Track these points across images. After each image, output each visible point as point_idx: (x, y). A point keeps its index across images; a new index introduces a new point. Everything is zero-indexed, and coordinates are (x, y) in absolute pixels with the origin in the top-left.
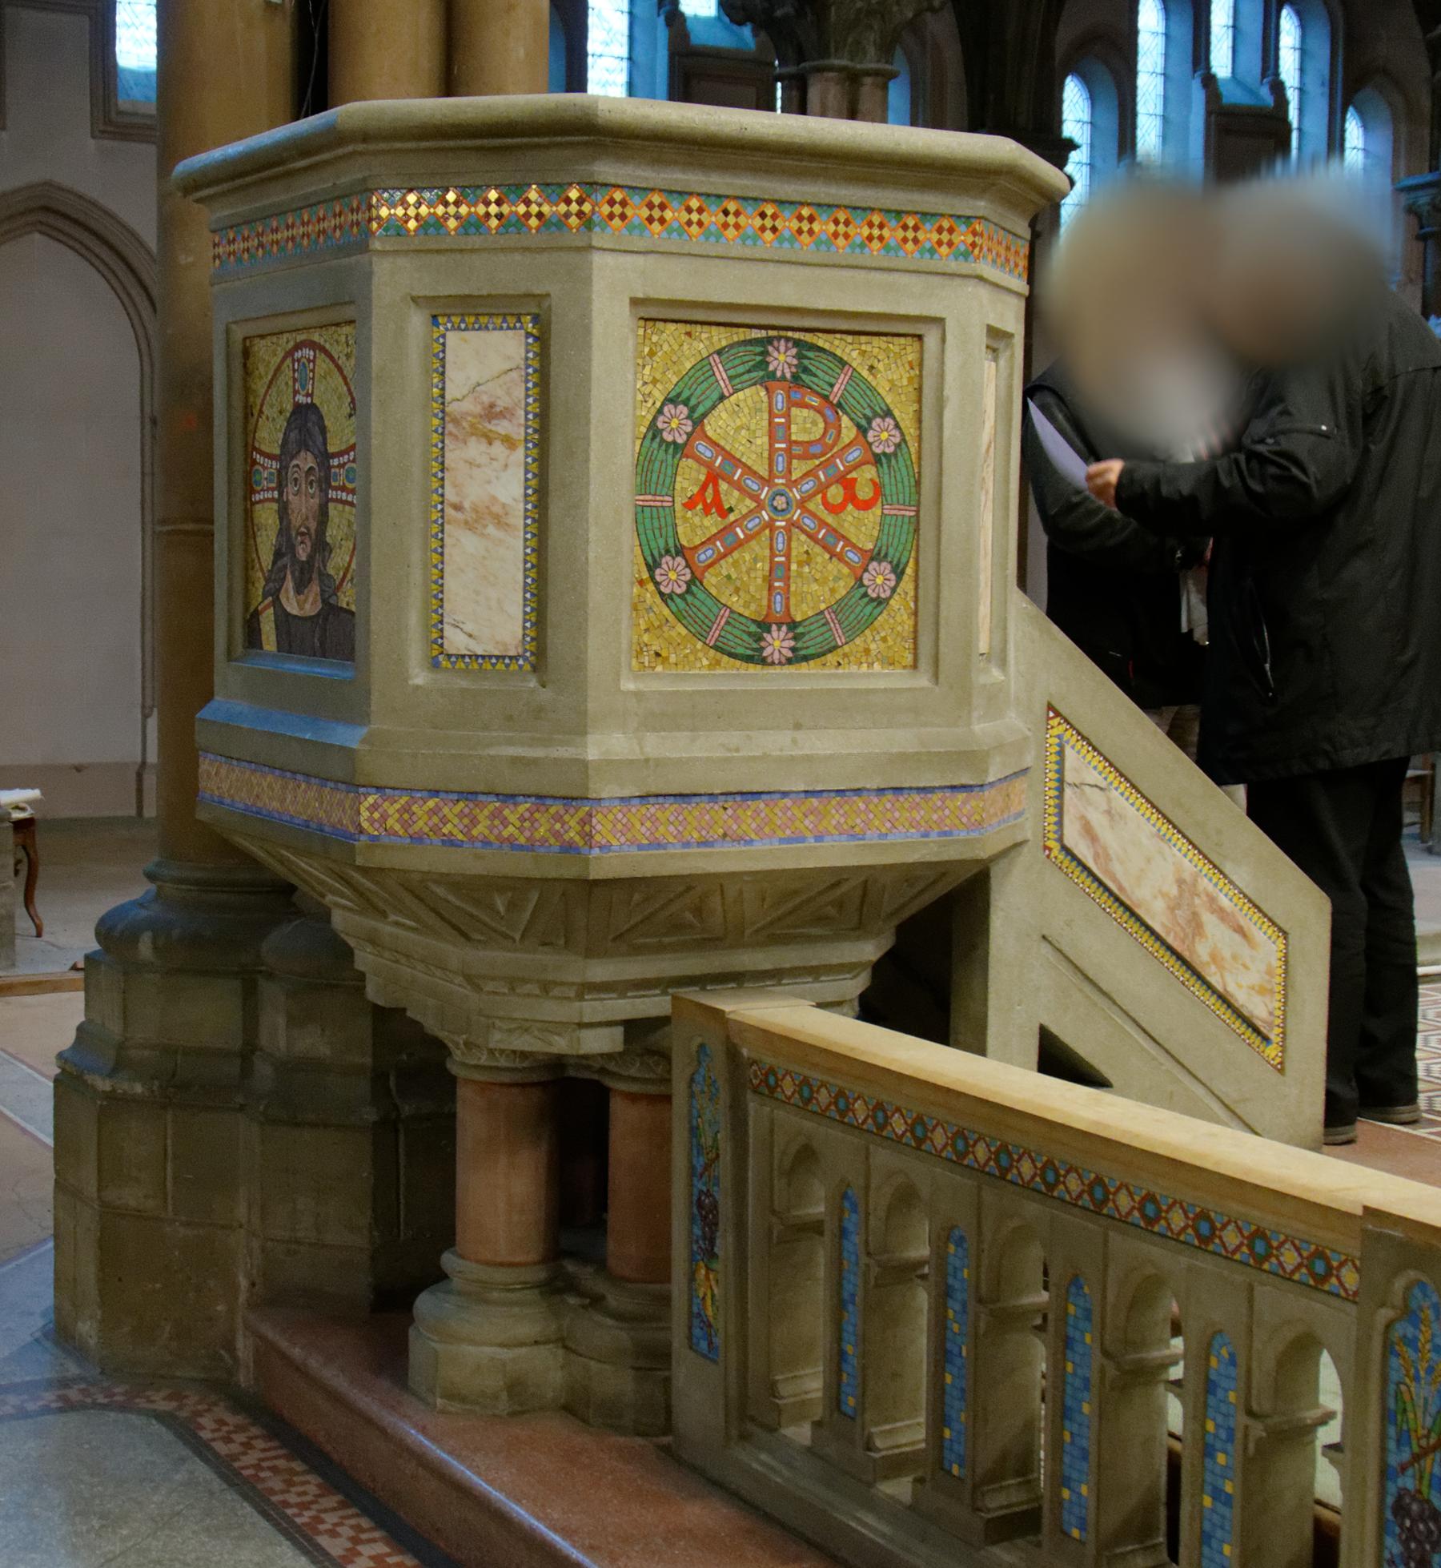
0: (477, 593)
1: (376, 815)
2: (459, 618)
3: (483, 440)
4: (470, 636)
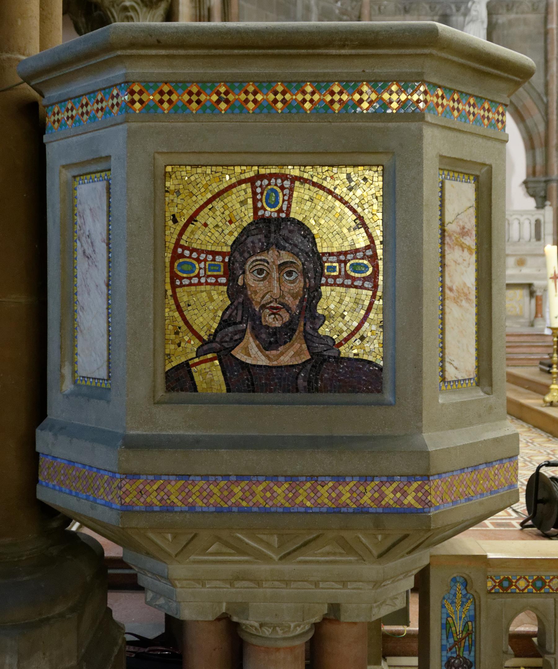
0: (459, 342)
1: (334, 495)
2: (452, 358)
3: (461, 248)
4: (456, 368)
